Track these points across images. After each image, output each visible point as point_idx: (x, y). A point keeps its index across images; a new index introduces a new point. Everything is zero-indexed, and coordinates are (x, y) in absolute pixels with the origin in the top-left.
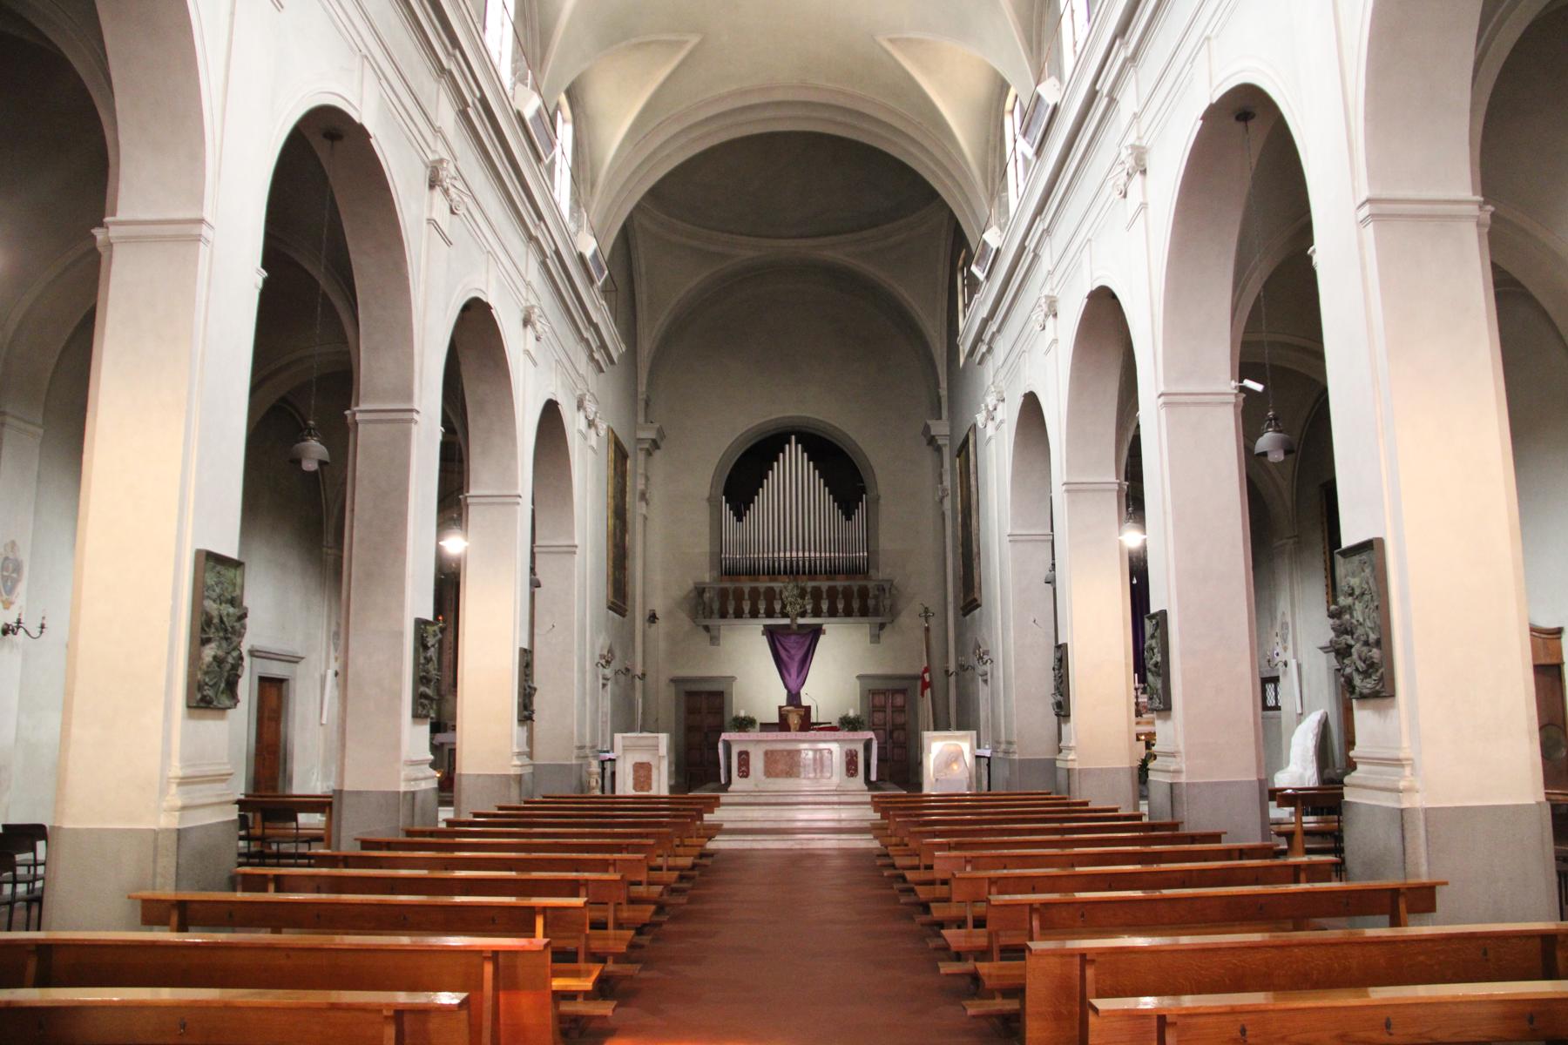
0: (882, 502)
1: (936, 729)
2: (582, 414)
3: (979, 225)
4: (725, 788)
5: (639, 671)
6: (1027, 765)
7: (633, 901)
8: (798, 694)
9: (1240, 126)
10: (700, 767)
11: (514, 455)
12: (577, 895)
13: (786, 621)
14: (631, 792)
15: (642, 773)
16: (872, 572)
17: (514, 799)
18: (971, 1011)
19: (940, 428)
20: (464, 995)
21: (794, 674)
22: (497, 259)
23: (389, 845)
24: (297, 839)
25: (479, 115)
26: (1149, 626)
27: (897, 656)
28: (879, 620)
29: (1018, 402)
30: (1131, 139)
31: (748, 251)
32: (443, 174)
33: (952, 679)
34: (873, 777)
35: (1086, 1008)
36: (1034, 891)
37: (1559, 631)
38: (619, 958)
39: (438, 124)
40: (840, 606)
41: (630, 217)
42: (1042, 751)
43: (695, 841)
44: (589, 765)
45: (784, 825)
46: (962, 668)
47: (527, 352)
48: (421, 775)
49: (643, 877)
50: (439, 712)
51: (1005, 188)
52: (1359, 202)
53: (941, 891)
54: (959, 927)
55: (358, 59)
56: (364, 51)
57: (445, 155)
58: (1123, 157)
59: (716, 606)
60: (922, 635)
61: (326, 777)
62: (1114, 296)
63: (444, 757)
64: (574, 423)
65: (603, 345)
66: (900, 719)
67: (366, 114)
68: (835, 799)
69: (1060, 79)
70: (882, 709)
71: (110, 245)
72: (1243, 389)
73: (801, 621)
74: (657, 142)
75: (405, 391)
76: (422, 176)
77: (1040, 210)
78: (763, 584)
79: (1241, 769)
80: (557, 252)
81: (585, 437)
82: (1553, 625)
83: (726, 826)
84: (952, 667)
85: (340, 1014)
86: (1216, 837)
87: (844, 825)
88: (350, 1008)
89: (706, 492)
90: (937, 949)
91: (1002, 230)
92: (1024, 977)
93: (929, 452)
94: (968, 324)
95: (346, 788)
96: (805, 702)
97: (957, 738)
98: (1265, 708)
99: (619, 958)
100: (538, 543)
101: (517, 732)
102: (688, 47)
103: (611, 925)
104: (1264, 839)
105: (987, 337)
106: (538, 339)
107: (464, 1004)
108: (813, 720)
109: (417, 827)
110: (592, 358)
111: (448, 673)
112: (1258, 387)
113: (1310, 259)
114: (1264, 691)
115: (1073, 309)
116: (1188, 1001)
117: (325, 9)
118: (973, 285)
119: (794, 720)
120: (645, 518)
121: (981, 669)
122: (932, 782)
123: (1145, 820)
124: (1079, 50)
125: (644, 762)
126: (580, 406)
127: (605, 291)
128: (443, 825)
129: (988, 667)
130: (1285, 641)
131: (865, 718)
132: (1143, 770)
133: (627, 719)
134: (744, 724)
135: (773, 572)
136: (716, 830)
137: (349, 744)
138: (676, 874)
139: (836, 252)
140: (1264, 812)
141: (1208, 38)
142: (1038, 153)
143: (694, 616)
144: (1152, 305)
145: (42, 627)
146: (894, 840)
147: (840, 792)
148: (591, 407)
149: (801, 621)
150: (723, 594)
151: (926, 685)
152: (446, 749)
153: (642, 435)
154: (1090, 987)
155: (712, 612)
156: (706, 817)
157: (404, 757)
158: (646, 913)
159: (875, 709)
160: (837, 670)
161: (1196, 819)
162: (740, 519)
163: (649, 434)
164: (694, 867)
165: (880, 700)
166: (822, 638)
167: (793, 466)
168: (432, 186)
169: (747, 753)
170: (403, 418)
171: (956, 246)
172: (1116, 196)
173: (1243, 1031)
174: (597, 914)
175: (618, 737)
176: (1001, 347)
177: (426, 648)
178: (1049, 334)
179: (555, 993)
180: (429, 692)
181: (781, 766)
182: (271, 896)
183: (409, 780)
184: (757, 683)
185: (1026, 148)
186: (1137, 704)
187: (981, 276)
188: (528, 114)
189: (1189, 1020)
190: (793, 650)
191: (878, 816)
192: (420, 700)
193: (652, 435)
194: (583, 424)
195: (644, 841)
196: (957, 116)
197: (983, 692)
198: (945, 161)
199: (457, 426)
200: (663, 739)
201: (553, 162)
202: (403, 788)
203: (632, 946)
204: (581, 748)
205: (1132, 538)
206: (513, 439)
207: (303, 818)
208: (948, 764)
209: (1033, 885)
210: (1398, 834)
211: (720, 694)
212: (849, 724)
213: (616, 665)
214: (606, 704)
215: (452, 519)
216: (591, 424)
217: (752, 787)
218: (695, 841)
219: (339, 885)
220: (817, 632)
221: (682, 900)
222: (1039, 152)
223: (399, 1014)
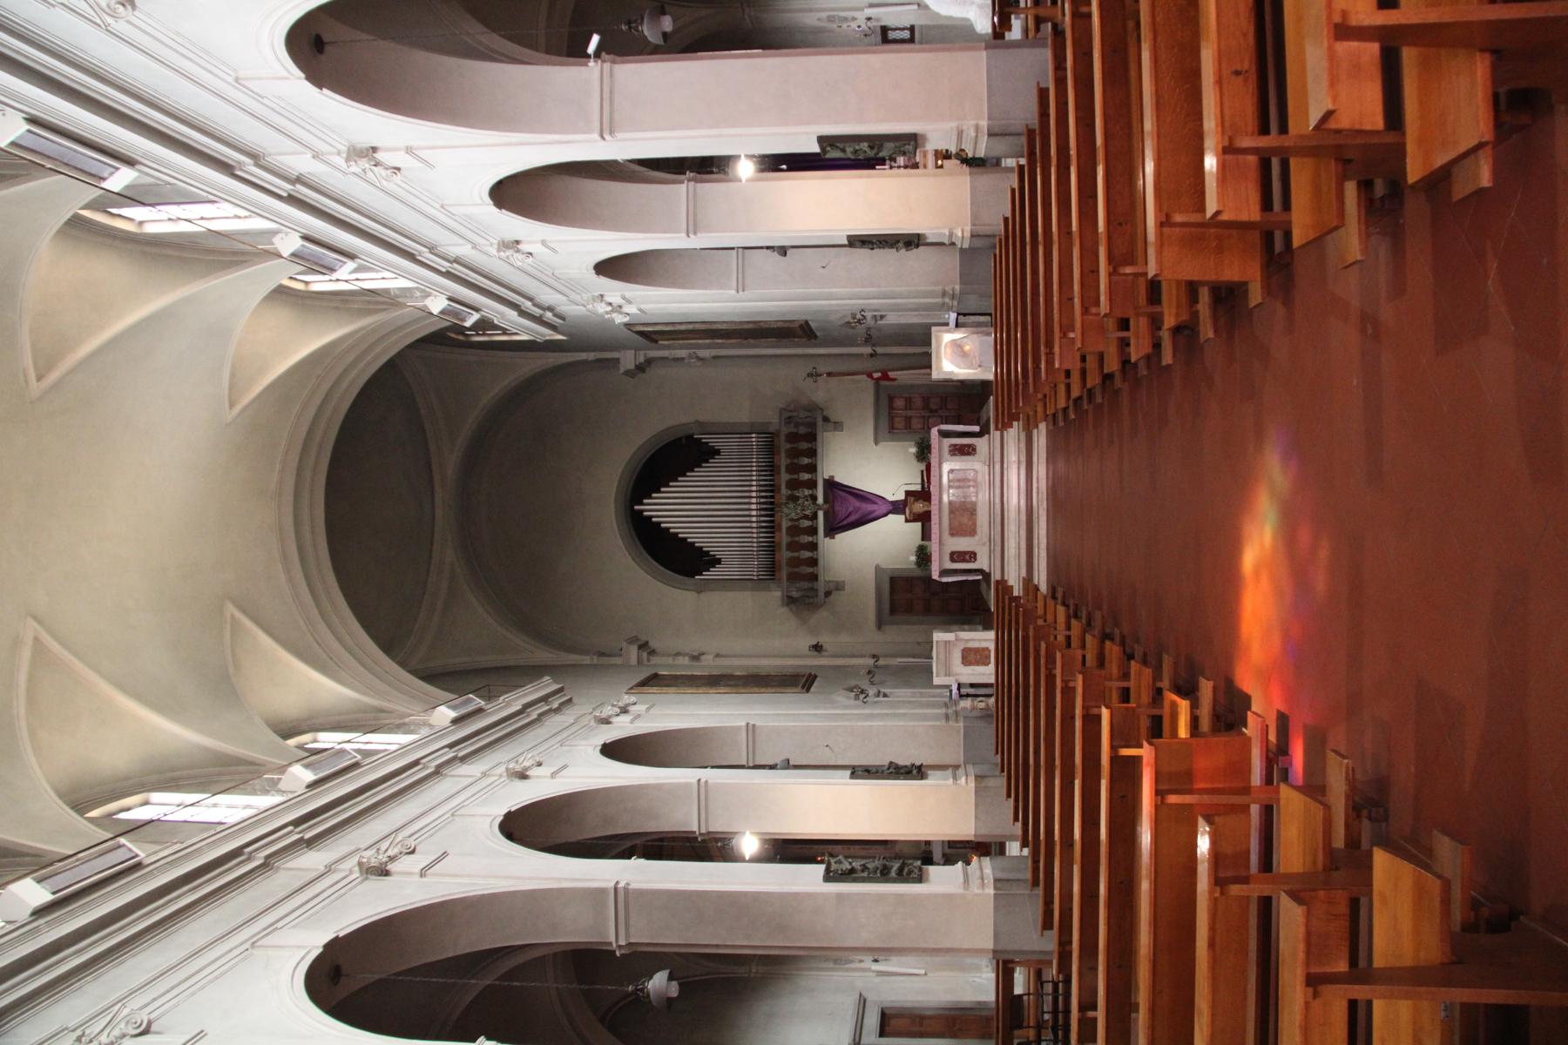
0: (702, 418)
1: (930, 367)
2: (614, 720)
3: (423, 318)
4: (986, 576)
5: (871, 662)
6: (964, 278)
7: (1101, 661)
8: (893, 503)
9: (328, 49)
10: (963, 601)
11: (659, 787)
12: (1099, 717)
13: (821, 514)
14: (991, 668)
15: (972, 657)
16: (771, 430)
17: (1000, 782)
18: (1211, 335)
19: (628, 360)
20: (1201, 821)
21: (874, 507)
22: (461, 806)
23: (1048, 902)
24: (1039, 995)
25: (312, 827)
26: (833, 154)
27: (856, 403)
29: (604, 281)
30: (340, 161)
31: (447, 554)
32: (374, 862)
33: (879, 350)
34: (976, 429)
35: (1215, 222)
36: (1096, 271)
38: (1157, 676)
39: (322, 869)
40: (806, 461)
41: (410, 672)
42: (953, 262)
43: (1040, 604)
44: (964, 709)
45: (1024, 518)
46: (869, 340)
47: (553, 775)
48: (978, 873)
49: (1079, 653)
50: (916, 858)
51: (386, 291)
53: (1091, 364)
54: (1128, 345)
55: (255, 952)
56: (247, 945)
57: (355, 860)
59: (806, 585)
60: (835, 379)
61: (977, 968)
62: (500, 183)
63: (957, 852)
64: (623, 727)
65: (545, 699)
66: (918, 402)
67: (311, 941)
68: (998, 467)
69: (275, 233)
70: (908, 420)
72: (597, 54)
73: (820, 500)
74: (336, 645)
75: (595, 896)
76: (376, 883)
78: (784, 538)
79: (974, 67)
80: (451, 746)
81: (638, 716)
83: (1024, 574)
84: (868, 350)
85: (1218, 939)
86: (1043, 93)
87: (1023, 458)
88: (1212, 929)
89: (690, 596)
90: (1148, 367)
91: (429, 295)
92: (1178, 283)
93: (654, 372)
94: (524, 331)
95: (990, 945)
96: (902, 497)
97: (939, 346)
98: (911, 40)
99: (1157, 676)
100: (744, 762)
101: (933, 780)
103: (1125, 684)
104: (1044, 46)
106: (540, 764)
107: (1209, 821)
108: (918, 488)
109: (1028, 875)
110: (557, 710)
111: (873, 850)
112: (595, 39)
114: (895, 41)
115: (512, 224)
116: (1210, 123)
117: (202, 988)
118: (484, 325)
119: (919, 507)
120: (717, 655)
121: (870, 322)
123: (1023, 161)
124: (243, 213)
125: (962, 656)
126: (606, 721)
127: (489, 698)
128: (1026, 851)
129: (869, 315)
130: (845, 19)
131: (917, 437)
132: (973, 163)
133: (918, 672)
134: (923, 556)
135: (772, 528)
136: (1028, 581)
137: (946, 944)
138: (1073, 621)
139: (449, 462)
140: (1015, 45)
141: (237, 80)
142: (352, 256)
144: (511, 144)
146: (1040, 409)
147: (991, 464)
148: (608, 711)
149: (820, 500)
150: (793, 577)
151: (885, 377)
152: (948, 851)
154: (1193, 218)
155: (812, 589)
156: (1016, 593)
157: (961, 891)
158: (1113, 650)
159: (908, 425)
160: (871, 465)
161: (1024, 112)
162: (719, 561)
163: (633, 651)
164: (1064, 604)
165: (899, 422)
166: (837, 479)
168: (387, 873)
169: (952, 554)
170: (623, 897)
171: (446, 343)
172: (398, 178)
173: (1237, 73)
174: (1115, 696)
175: (937, 681)
176: (547, 296)
177: (852, 871)
179: (1192, 735)
180: (896, 866)
181: (965, 520)
182: (1100, 1015)
183: (983, 885)
184: (882, 543)
185: (346, 270)
186: (906, 167)
187: (475, 317)
188: (310, 777)
189: (1227, 124)
190: (852, 508)
191: (1015, 424)
192: (904, 876)
193: (634, 650)
194: (625, 718)
195: (1043, 653)
196: (312, 339)
197: (892, 319)
199: (629, 844)
200: (938, 636)
201: (358, 751)
202: (991, 891)
203: (1145, 663)
204: (947, 717)
205: (745, 169)
206: (640, 787)
207: (1018, 990)
208: (964, 355)
209: (1090, 272)
211: (893, 580)
212: (924, 453)
213: (864, 684)
214: (902, 693)
215: (723, 847)
216: (624, 711)
217: (986, 549)
218: (1040, 604)
219: (1089, 949)
220: (831, 485)
221: (1098, 615)
222: (351, 256)
223: (1219, 881)
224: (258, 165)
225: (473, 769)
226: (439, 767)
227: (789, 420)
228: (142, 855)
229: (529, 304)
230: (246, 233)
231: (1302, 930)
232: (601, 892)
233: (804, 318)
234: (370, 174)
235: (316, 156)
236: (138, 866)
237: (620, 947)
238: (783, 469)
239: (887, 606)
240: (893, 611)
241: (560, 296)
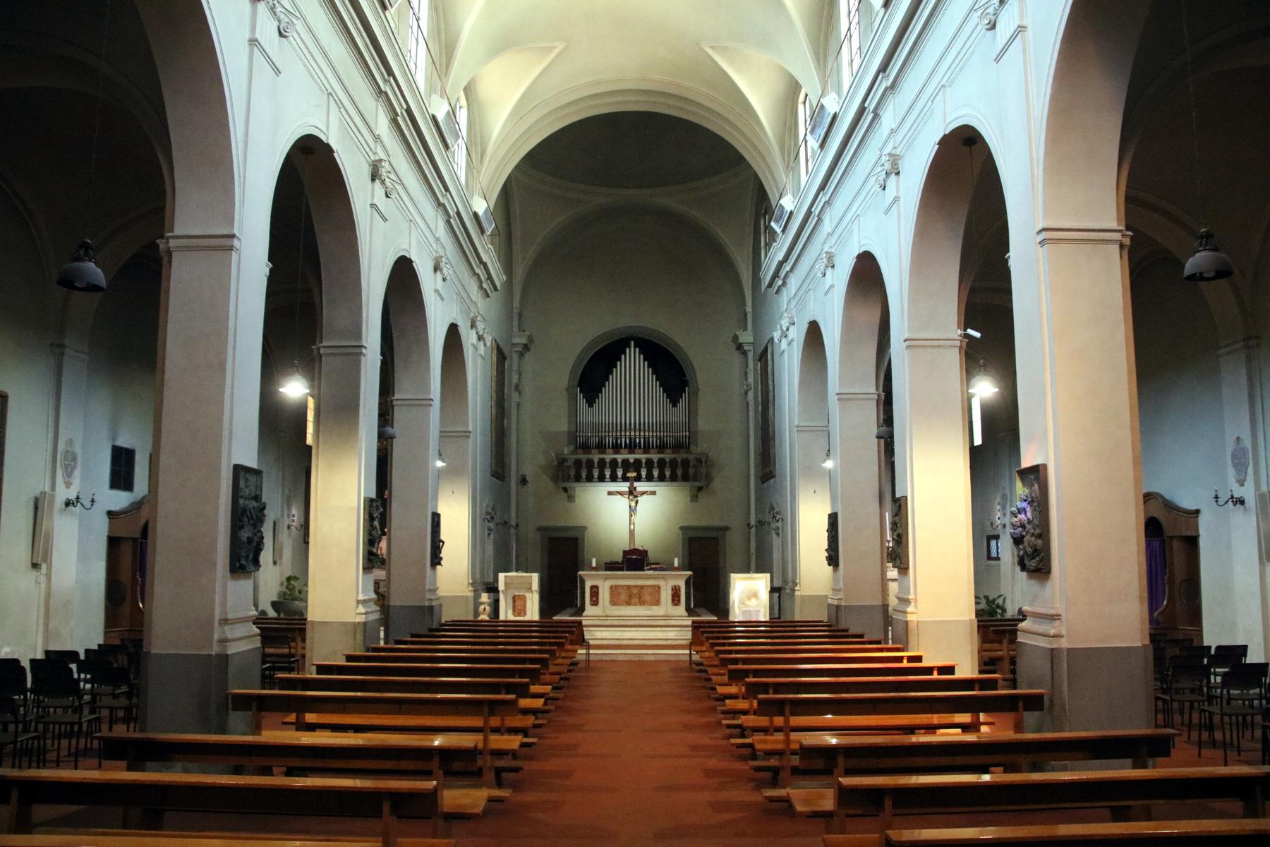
0: (700, 395)
2: (474, 332)
5: (513, 523)
9: (968, 149)
14: (511, 617)
16: (693, 448)
19: (746, 337)
25: (406, 124)
28: (697, 484)
29: (805, 327)
30: (888, 149)
33: (753, 530)
37: (1197, 512)
40: (668, 473)
46: (760, 523)
47: (437, 291)
52: (1038, 229)
57: (383, 156)
58: (884, 159)
59: (572, 473)
64: (469, 338)
65: (490, 278)
68: (664, 623)
69: (839, 95)
71: (169, 253)
75: (356, 331)
76: (366, 171)
77: (823, 187)
80: (458, 213)
81: (476, 348)
82: (1194, 508)
84: (753, 522)
89: (564, 381)
91: (794, 197)
93: (737, 357)
102: (556, 51)
105: (782, 274)
106: (444, 280)
110: (481, 287)
112: (978, 335)
113: (1006, 261)
115: (845, 265)
121: (774, 526)
122: (738, 612)
125: (522, 597)
126: (473, 325)
129: (780, 524)
141: (943, 86)
143: (555, 479)
145: (93, 501)
148: (480, 326)
150: (578, 463)
153: (516, 340)
162: (591, 405)
163: (520, 340)
167: (632, 366)
168: (373, 180)
169: (597, 587)
172: (877, 188)
175: (501, 576)
176: (793, 282)
178: (829, 280)
185: (813, 143)
187: (779, 230)
188: (441, 117)
193: (524, 341)
196: (760, 98)
197: (776, 542)
198: (749, 135)
200: (535, 577)
210: (1049, 665)
213: (497, 518)
216: (480, 338)
224: (886, 89)
225: (441, 231)
226: (443, 206)
227: (699, 461)
228: (392, 10)
229: (788, 268)
230: (839, 20)
231: (855, 603)
232: (359, 337)
233: (778, 473)
234: (879, 169)
235: (893, 132)
236: (384, 8)
237: (319, 349)
238: (662, 456)
239: (555, 535)
240: (551, 539)
241: (793, 292)
